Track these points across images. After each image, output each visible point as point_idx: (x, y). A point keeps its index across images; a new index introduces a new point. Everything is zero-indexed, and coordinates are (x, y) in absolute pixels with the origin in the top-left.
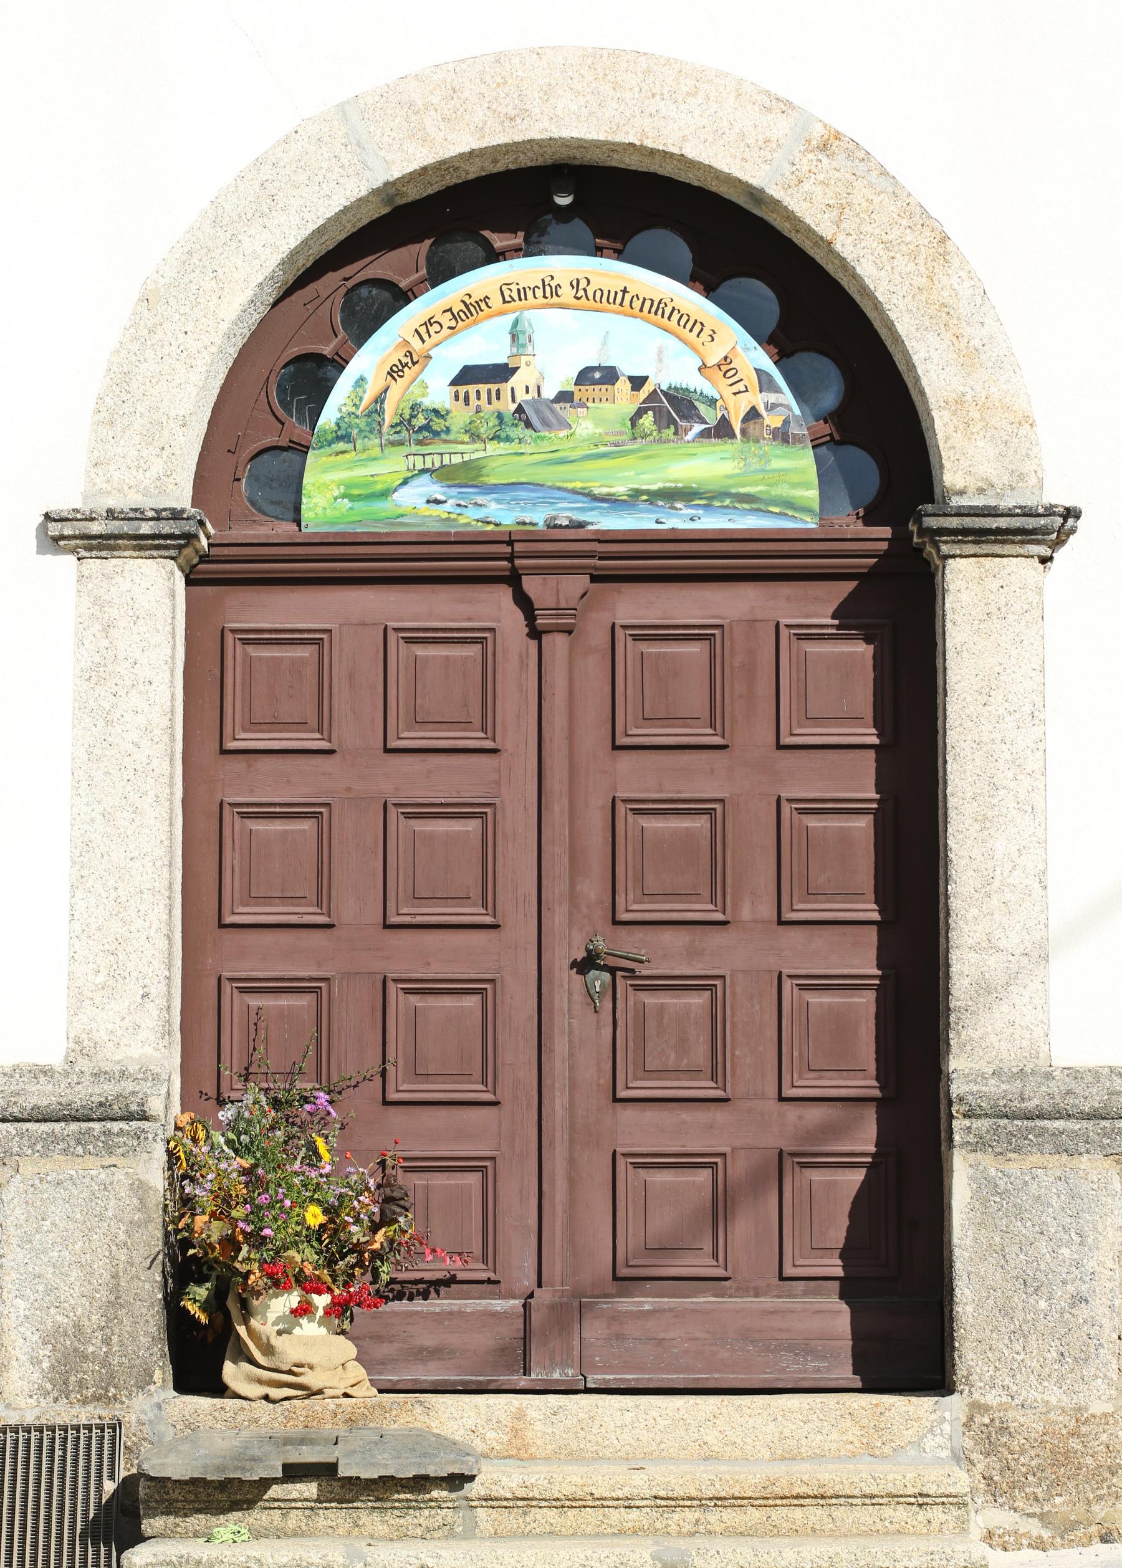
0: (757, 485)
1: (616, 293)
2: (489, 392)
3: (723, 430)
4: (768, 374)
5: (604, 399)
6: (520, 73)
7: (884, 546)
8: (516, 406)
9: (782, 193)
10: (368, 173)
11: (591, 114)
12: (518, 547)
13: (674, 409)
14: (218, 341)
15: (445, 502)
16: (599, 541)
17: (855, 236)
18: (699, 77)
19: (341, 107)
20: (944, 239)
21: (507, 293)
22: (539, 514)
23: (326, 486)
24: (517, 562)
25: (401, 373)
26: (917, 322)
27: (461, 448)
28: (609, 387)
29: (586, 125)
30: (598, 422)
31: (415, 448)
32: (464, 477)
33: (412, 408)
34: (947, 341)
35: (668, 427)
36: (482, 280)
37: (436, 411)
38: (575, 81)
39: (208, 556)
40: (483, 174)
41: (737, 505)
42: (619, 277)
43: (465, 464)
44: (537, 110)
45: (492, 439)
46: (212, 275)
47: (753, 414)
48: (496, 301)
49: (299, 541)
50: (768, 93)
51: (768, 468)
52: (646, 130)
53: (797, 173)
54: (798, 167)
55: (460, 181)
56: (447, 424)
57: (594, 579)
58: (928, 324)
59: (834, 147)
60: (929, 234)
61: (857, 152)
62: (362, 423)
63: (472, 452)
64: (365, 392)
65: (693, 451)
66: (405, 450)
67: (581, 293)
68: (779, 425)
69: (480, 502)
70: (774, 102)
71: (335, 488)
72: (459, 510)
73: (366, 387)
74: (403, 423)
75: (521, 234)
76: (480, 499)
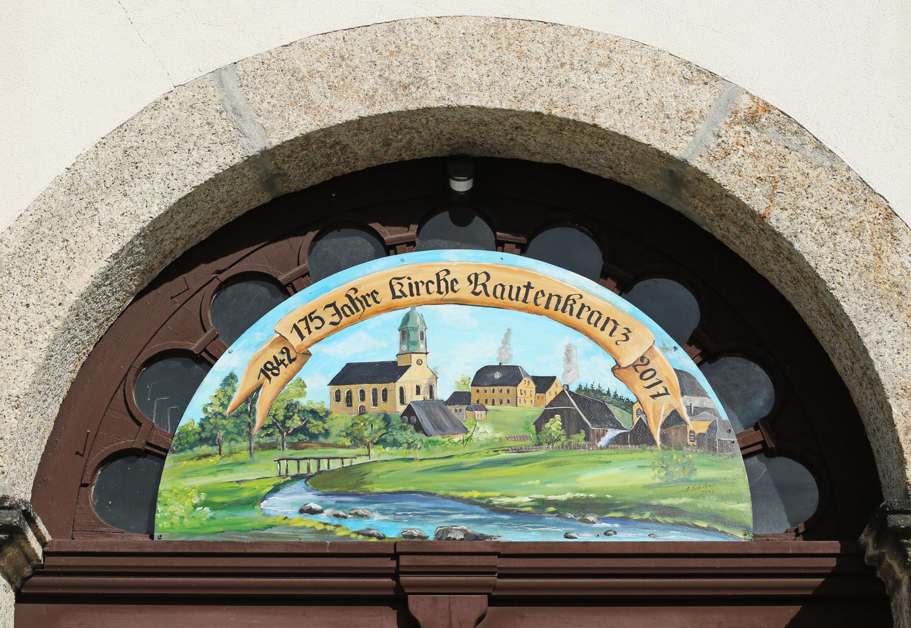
0: (681, 497)
1: (519, 288)
2: (375, 392)
3: (640, 436)
4: (689, 376)
5: (505, 401)
6: (416, 42)
7: (832, 562)
8: (404, 407)
9: (707, 165)
10: (244, 141)
11: (492, 83)
12: (404, 561)
13: (582, 414)
14: (63, 313)
15: (321, 512)
16: (500, 555)
17: (791, 211)
18: (612, 47)
19: (217, 73)
20: (891, 215)
21: (397, 288)
22: (430, 527)
23: (185, 492)
24: (403, 579)
25: (275, 371)
26: (866, 302)
27: (341, 452)
28: (511, 388)
29: (487, 94)
30: (497, 425)
31: (288, 453)
32: (344, 485)
33: (287, 409)
34: (901, 323)
35: (578, 432)
36: (373, 274)
37: (314, 412)
38: (476, 50)
39: (42, 567)
40: (374, 163)
41: (659, 519)
42: (521, 271)
43: (345, 469)
44: (434, 78)
45: (377, 443)
46: (61, 244)
47: (674, 419)
48: (385, 296)
49: (149, 550)
50: (688, 64)
51: (693, 478)
52: (555, 99)
53: (723, 145)
54: (724, 138)
55: (348, 171)
56: (326, 426)
57: (494, 601)
58: (878, 304)
59: (763, 120)
60: (873, 210)
61: (786, 123)
62: (229, 424)
63: (356, 457)
64: (234, 391)
65: (608, 458)
66: (277, 454)
67: (480, 288)
68: (704, 431)
69: (361, 512)
70: (695, 74)
71: (195, 495)
72: (336, 522)
73: (236, 385)
74: (276, 425)
75: (414, 227)
76: (361, 509)
